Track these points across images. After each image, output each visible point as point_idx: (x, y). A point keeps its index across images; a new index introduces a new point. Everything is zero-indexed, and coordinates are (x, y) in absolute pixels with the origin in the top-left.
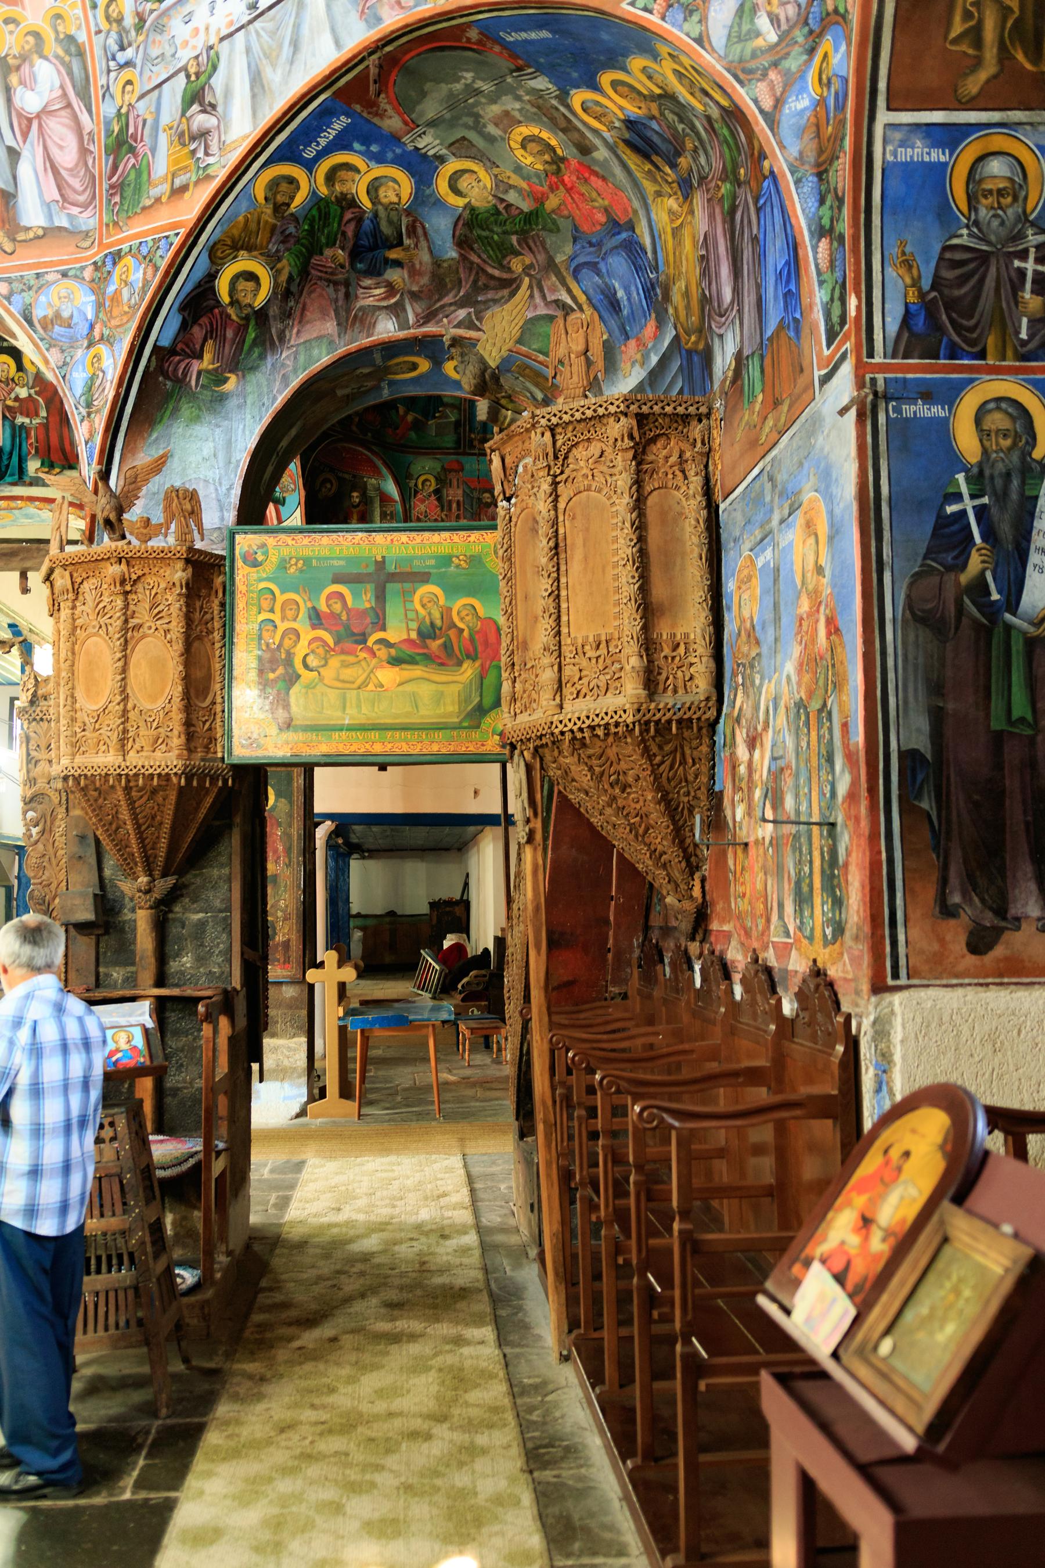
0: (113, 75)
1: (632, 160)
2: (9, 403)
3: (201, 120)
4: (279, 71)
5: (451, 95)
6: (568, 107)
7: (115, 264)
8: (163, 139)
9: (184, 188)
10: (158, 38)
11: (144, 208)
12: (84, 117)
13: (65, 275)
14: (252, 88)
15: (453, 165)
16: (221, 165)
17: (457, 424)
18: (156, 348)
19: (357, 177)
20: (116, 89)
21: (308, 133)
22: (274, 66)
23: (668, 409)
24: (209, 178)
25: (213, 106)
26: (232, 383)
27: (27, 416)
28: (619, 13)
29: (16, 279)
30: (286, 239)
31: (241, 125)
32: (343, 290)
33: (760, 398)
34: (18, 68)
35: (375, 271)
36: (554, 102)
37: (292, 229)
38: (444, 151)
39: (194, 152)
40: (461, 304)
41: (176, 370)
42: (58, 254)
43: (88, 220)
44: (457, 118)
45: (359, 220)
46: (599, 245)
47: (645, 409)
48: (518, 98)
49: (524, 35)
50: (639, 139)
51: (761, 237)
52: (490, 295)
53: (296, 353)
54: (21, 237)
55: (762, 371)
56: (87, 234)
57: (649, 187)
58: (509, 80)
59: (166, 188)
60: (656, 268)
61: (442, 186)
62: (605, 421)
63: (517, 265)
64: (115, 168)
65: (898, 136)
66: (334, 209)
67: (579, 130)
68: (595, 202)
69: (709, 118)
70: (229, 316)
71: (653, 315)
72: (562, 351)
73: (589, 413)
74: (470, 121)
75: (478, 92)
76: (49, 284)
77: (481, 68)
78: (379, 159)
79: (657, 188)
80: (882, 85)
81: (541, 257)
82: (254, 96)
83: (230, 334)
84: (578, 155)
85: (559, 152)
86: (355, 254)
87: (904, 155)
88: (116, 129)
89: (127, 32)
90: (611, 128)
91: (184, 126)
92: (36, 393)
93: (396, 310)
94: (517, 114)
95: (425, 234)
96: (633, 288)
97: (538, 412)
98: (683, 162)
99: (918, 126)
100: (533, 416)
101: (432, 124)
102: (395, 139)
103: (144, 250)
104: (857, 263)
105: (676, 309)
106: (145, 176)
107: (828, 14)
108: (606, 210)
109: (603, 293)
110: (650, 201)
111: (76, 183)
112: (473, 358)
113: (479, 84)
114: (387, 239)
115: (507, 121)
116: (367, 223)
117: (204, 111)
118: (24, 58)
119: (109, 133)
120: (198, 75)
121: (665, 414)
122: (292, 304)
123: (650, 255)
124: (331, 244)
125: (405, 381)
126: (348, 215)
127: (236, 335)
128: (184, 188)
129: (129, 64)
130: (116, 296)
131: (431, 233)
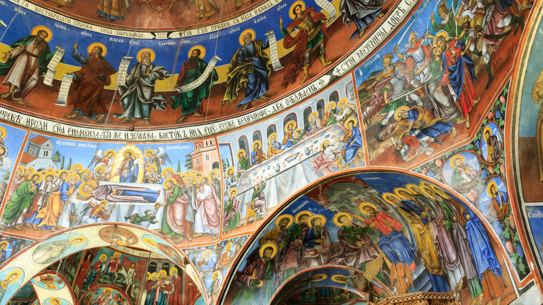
0: (228, 189)
1: (403, 213)
2: (162, 286)
3: (258, 202)
4: (287, 189)
5: (342, 194)
6: (381, 198)
7: (225, 244)
8: (245, 207)
9: (252, 222)
10: (245, 179)
11: (237, 228)
12: (218, 201)
13: (207, 248)
14: (277, 193)
15: (340, 214)
16: (266, 216)
17: (316, 294)
18: (238, 272)
19: (308, 218)
20: (229, 193)
21: (295, 205)
22: (285, 187)
23: (439, 297)
24: (261, 219)
25: (263, 198)
26: (261, 284)
27: (168, 290)
28: (409, 173)
29: (191, 249)
30: (283, 237)
31: (273, 203)
32: (300, 252)
33: (482, 295)
34: (199, 187)
35: (311, 246)
36: (377, 196)
37: (285, 234)
38: (337, 210)
39: (256, 211)
40: (340, 257)
41: (243, 279)
42: (206, 241)
43: (216, 231)
44: (342, 201)
45: (307, 231)
46: (390, 238)
47: (431, 297)
48: (364, 195)
49: (371, 178)
50: (407, 207)
51: (469, 239)
52: (350, 254)
53: (284, 273)
54: (194, 236)
55: (481, 285)
56: (216, 235)
57: (409, 221)
58: (362, 190)
59: (246, 221)
60: (414, 246)
61: (335, 220)
62: (415, 302)
63: (359, 244)
64: (227, 215)
65: (531, 210)
66: (300, 227)
67: (384, 204)
68: (389, 225)
69: (437, 202)
70: (262, 261)
71: (414, 262)
72: (395, 276)
73: (409, 299)
74: (347, 201)
75: (351, 193)
76: (202, 251)
77: (353, 188)
78: (316, 212)
79: (412, 221)
80: (521, 195)
81: (368, 242)
82: (278, 195)
83: (262, 267)
84: (383, 211)
85: (376, 210)
86: (305, 241)
87: (535, 216)
88: (228, 204)
89: (234, 178)
90: (396, 203)
91: (253, 203)
92: (172, 283)
93: (318, 259)
94: (363, 200)
95: (328, 235)
96: (404, 252)
97: (389, 298)
98: (424, 214)
99: (537, 207)
100: (387, 300)
101: (334, 202)
102: (322, 207)
103: (237, 240)
104: (529, 250)
105: (425, 260)
106: (238, 218)
107: (490, 174)
108: (392, 227)
109: (391, 253)
110: (409, 225)
111: (214, 220)
112: (363, 278)
113: (352, 191)
114: (316, 236)
115: (360, 201)
116: (310, 232)
117: (260, 199)
118: (201, 185)
119: (226, 205)
120: (258, 189)
121: (439, 299)
122: (283, 257)
123: (410, 241)
124: (297, 238)
125: (317, 282)
126: (304, 229)
127: (264, 267)
128: (252, 222)
129: (234, 186)
130: (225, 255)
131: (330, 234)
